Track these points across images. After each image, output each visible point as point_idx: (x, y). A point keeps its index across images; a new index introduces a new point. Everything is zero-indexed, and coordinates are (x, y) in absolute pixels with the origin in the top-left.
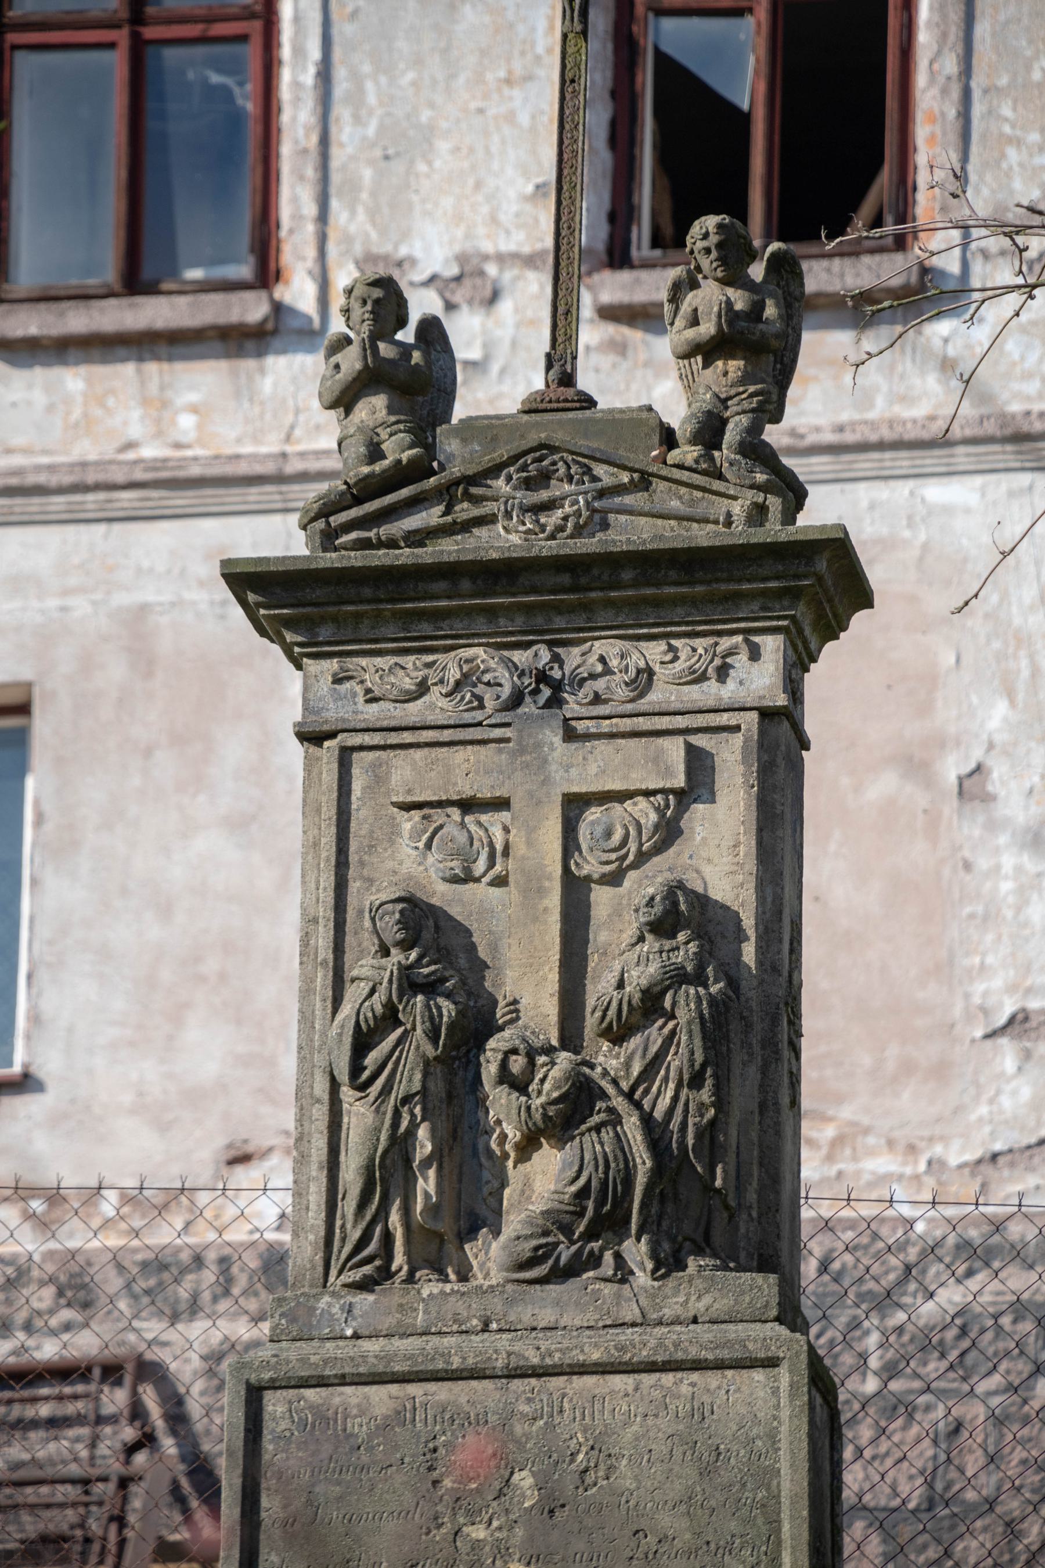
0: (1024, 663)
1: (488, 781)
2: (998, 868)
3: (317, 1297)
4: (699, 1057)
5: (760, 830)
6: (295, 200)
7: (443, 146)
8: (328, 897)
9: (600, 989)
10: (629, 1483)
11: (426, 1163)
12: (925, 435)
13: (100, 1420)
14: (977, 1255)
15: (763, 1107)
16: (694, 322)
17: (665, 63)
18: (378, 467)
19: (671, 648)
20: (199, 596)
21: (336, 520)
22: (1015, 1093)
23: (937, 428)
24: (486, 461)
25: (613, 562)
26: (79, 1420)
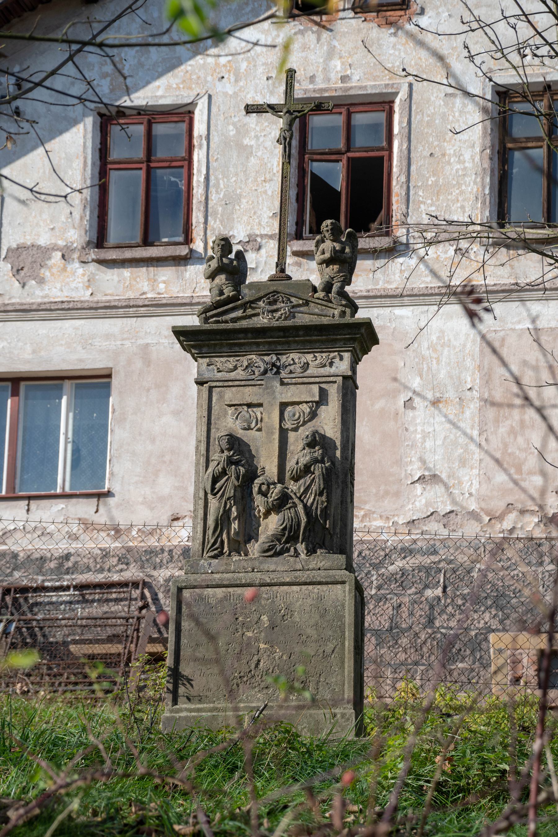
0: (425, 366)
1: (256, 398)
2: (416, 430)
3: (200, 560)
4: (322, 486)
5: (342, 414)
6: (197, 217)
7: (244, 201)
8: (204, 434)
9: (291, 464)
10: (298, 620)
11: (235, 519)
12: (395, 293)
13: (131, 599)
14: (407, 552)
15: (342, 502)
16: (323, 253)
17: (314, 177)
18: (222, 298)
19: (315, 356)
20: (165, 341)
21: (209, 314)
22: (420, 501)
23: (399, 291)
24: (257, 296)
25: (296, 329)
26: (126, 599)
